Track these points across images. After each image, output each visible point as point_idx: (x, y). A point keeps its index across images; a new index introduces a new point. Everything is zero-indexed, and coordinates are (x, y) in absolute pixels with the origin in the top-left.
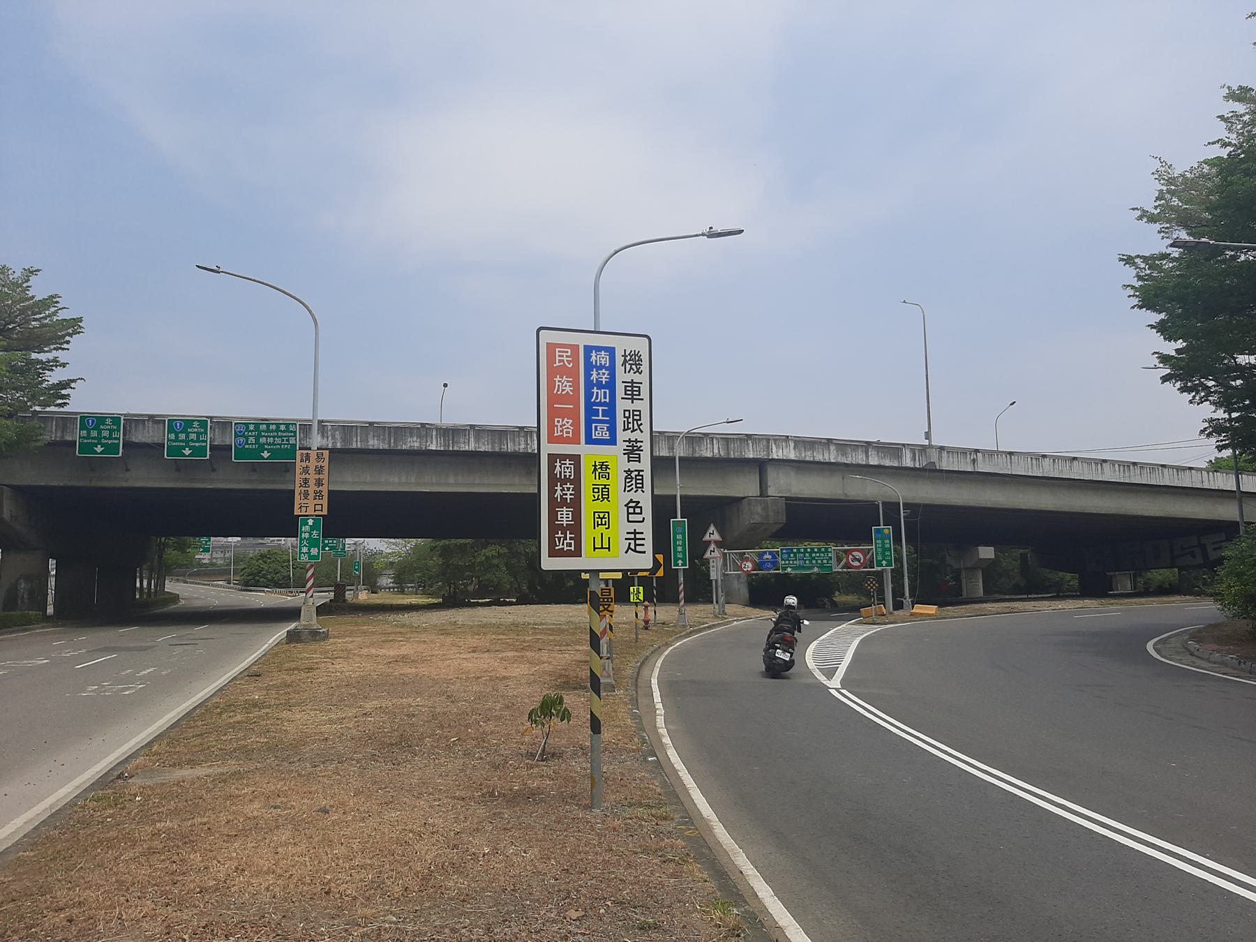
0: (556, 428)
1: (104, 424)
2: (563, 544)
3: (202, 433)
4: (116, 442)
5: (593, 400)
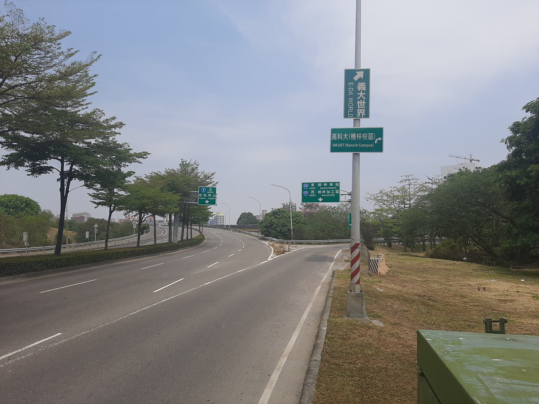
1: (209, 191)
3: (213, 194)
4: (214, 199)
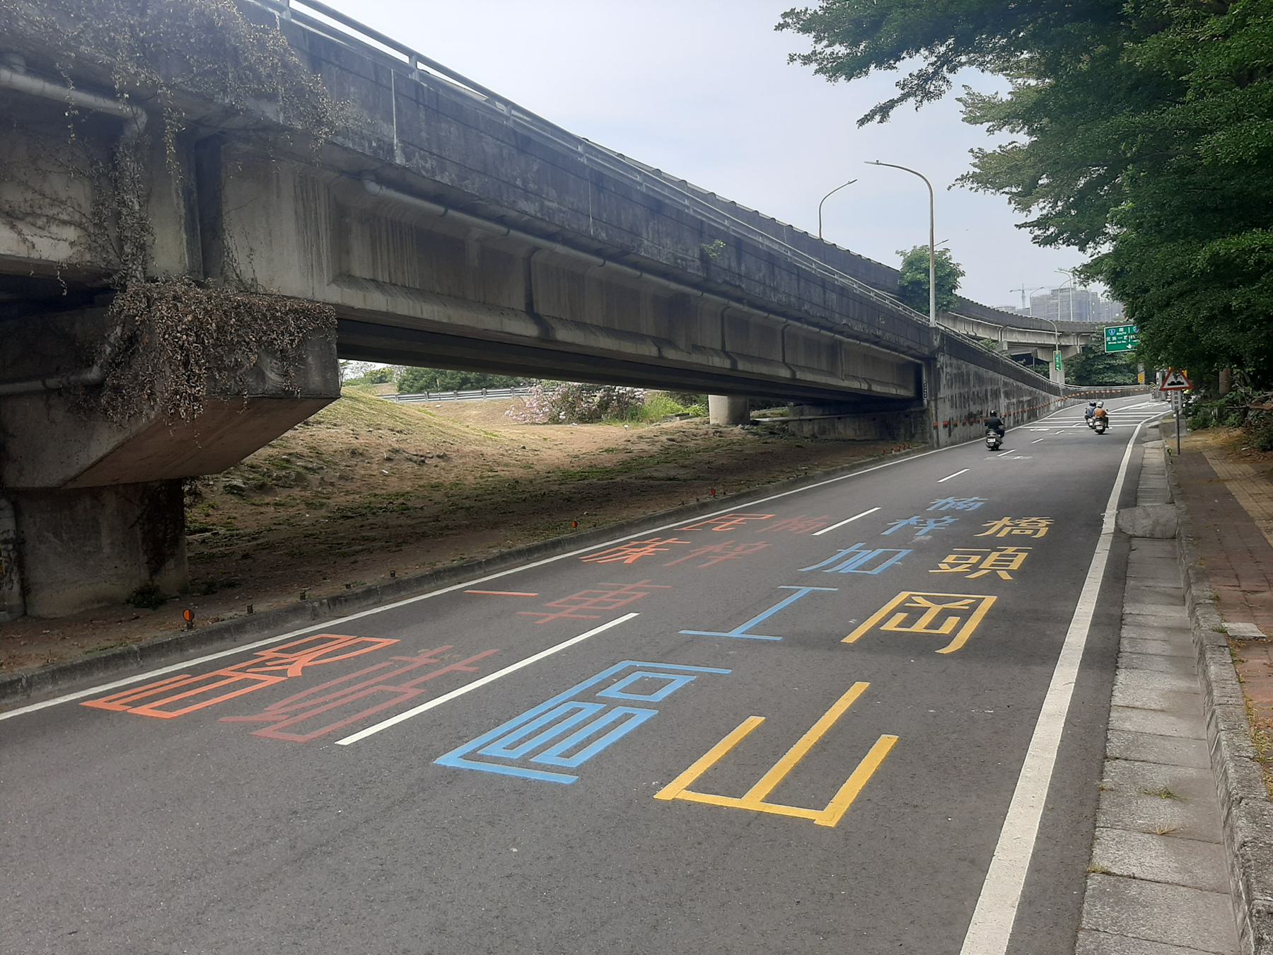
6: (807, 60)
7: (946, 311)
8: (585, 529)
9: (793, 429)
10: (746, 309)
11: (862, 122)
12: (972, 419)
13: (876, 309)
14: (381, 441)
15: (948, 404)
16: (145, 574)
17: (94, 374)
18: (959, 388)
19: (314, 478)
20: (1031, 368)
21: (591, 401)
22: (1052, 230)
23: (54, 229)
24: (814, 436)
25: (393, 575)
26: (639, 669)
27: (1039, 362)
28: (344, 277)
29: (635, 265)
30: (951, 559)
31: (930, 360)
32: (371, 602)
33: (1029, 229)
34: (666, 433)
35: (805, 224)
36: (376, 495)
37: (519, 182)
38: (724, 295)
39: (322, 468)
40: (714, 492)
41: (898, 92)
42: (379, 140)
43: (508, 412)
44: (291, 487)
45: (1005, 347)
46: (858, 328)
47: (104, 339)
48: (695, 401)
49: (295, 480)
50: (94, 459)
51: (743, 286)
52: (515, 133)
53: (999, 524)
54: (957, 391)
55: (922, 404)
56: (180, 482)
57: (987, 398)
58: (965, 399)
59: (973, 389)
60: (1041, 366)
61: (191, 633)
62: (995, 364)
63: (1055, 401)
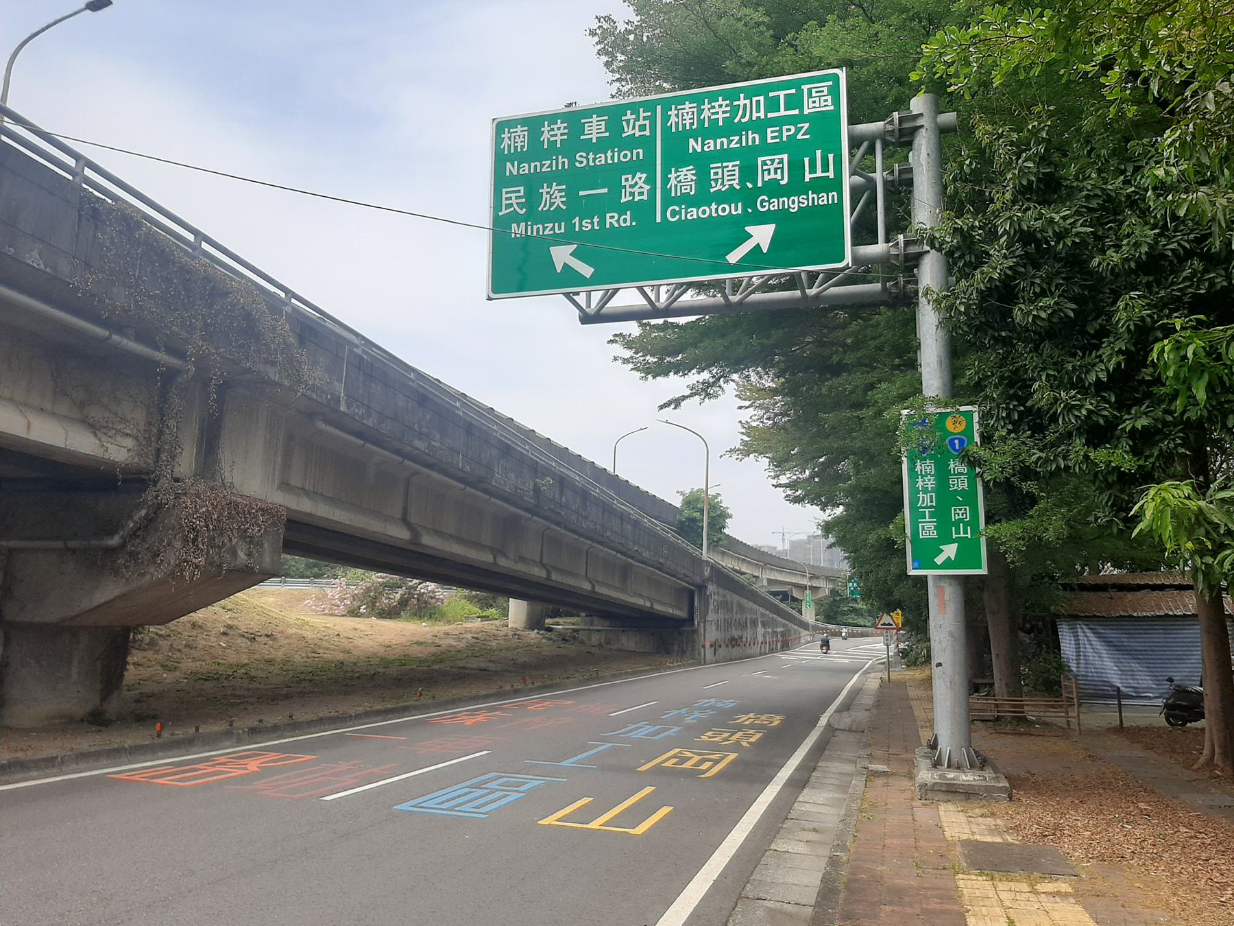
0: (623, 190)
2: (634, 128)
5: (736, 121)
6: (626, 361)
7: (717, 546)
8: (424, 700)
9: (583, 638)
10: (563, 531)
11: (661, 407)
12: (734, 643)
13: (662, 541)
14: (216, 617)
15: (714, 627)
16: (97, 700)
17: (115, 541)
18: (724, 614)
19: (164, 644)
20: (787, 604)
21: (392, 597)
22: (800, 492)
23: (118, 438)
24: (600, 645)
25: (291, 717)
26: (504, 777)
27: (794, 599)
28: (285, 486)
29: (486, 491)
30: (709, 734)
31: (702, 588)
32: (275, 735)
33: (782, 489)
34: (470, 632)
35: (603, 461)
36: (219, 664)
37: (416, 427)
38: (547, 518)
39: (169, 636)
40: (525, 682)
41: (688, 392)
42: (332, 394)
43: (307, 601)
44: (144, 650)
45: (765, 583)
46: (646, 554)
47: (130, 517)
48: (491, 605)
49: (148, 644)
50: (95, 604)
51: (563, 513)
52: (418, 392)
53: (745, 717)
54: (722, 617)
55: (693, 625)
56: (127, 630)
57: (746, 626)
58: (728, 624)
59: (735, 617)
60: (796, 603)
61: (160, 740)
62: (753, 596)
63: (805, 635)
